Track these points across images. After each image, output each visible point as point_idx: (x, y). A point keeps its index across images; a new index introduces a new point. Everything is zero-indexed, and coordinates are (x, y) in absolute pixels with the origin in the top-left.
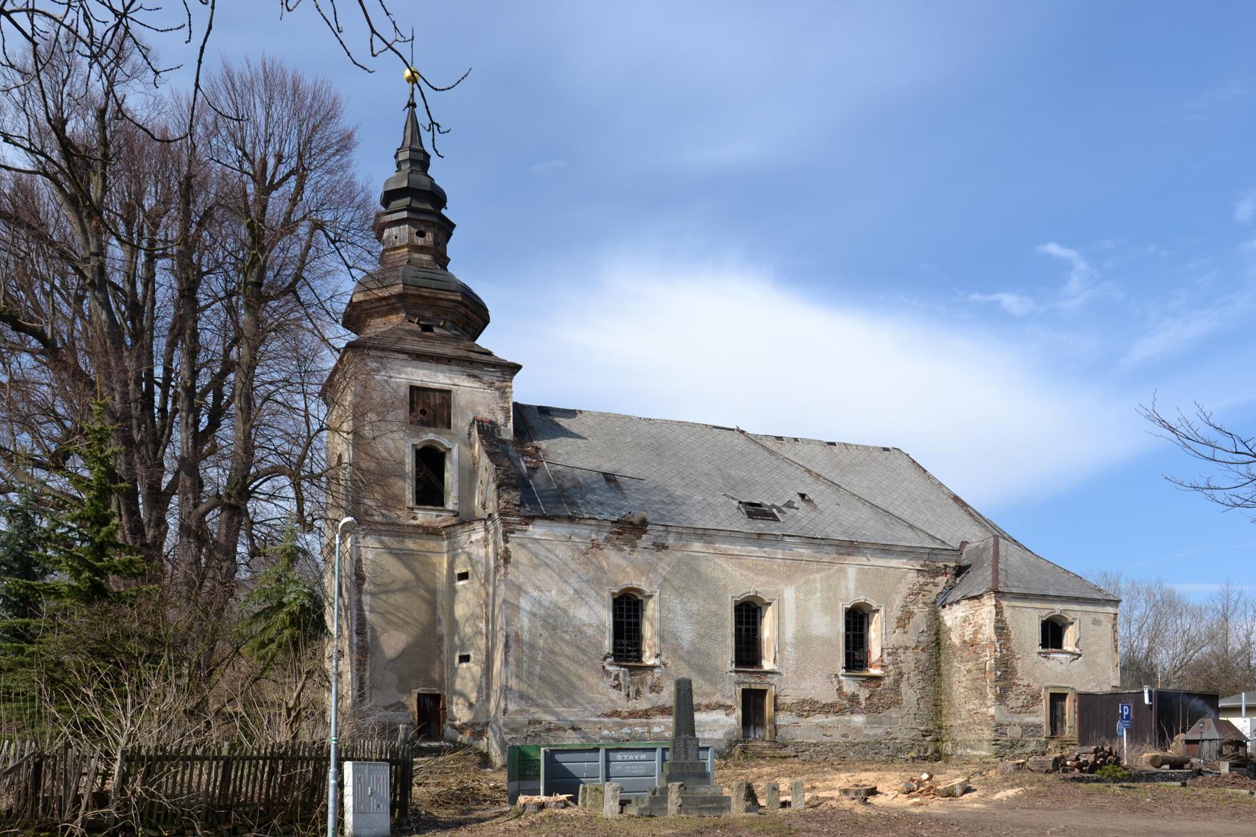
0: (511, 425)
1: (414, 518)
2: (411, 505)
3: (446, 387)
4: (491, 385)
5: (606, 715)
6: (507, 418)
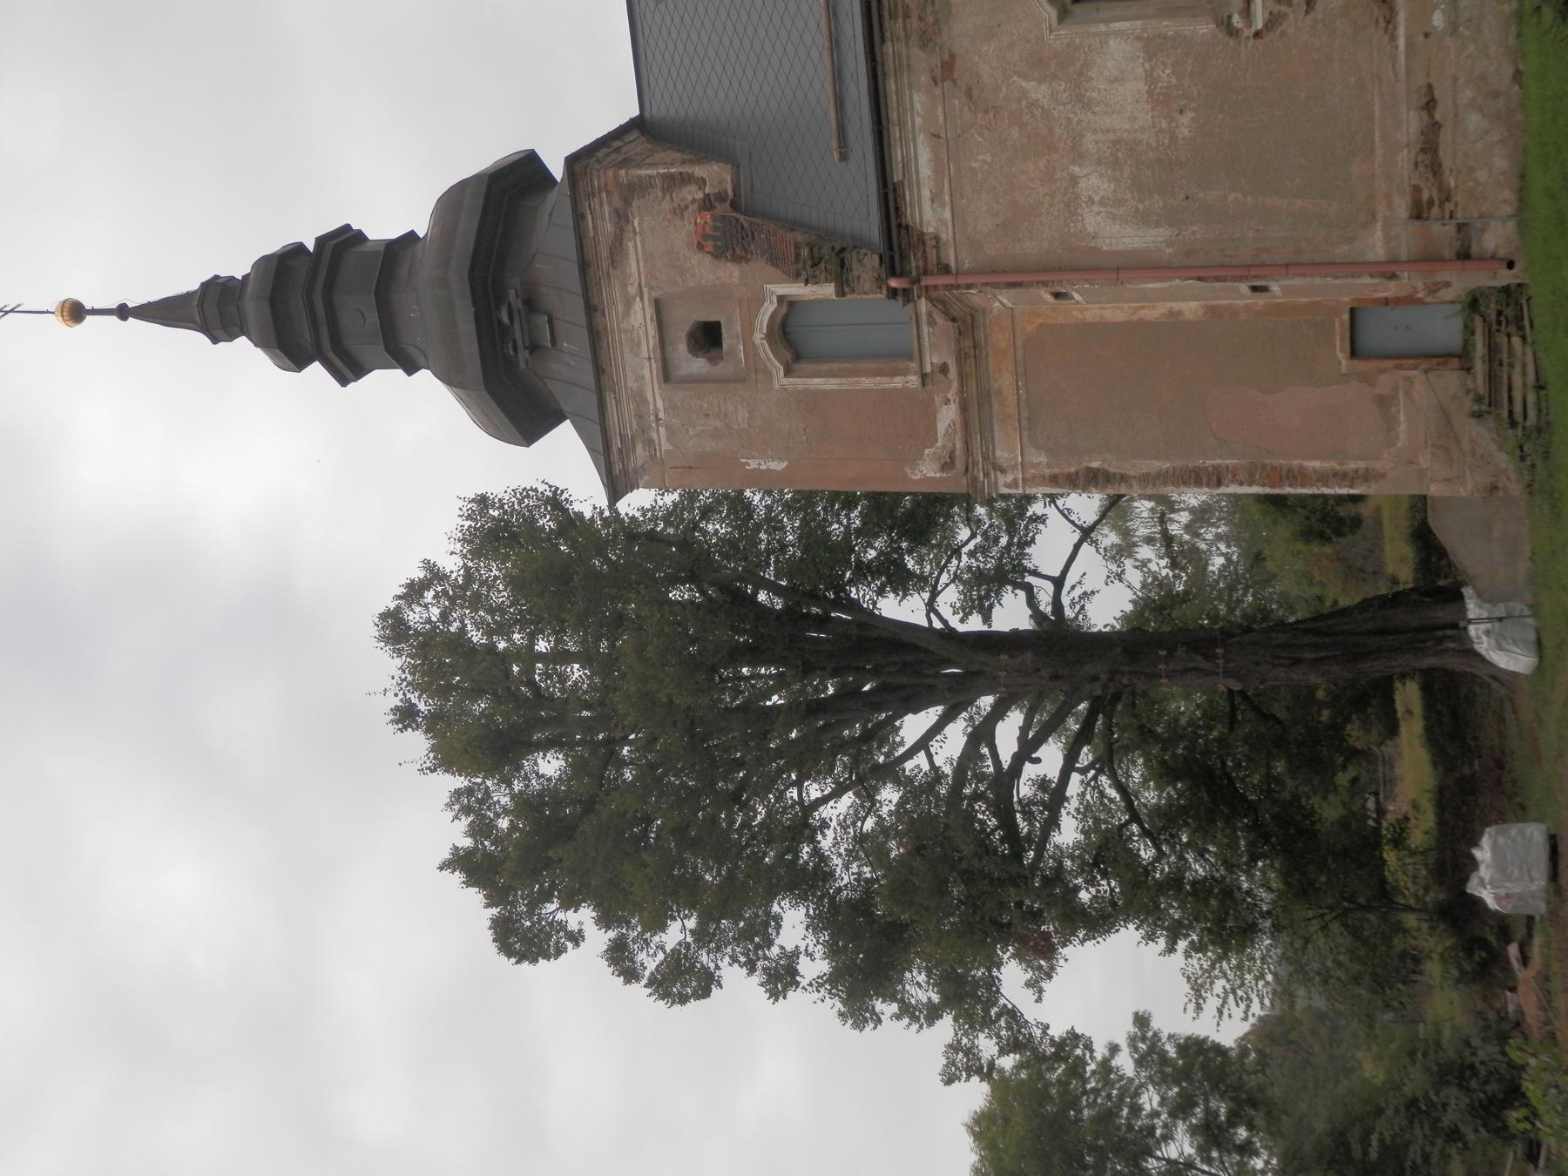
0: (699, 171)
1: (944, 369)
2: (914, 380)
3: (650, 311)
4: (622, 218)
5: (1390, 20)
6: (686, 179)
